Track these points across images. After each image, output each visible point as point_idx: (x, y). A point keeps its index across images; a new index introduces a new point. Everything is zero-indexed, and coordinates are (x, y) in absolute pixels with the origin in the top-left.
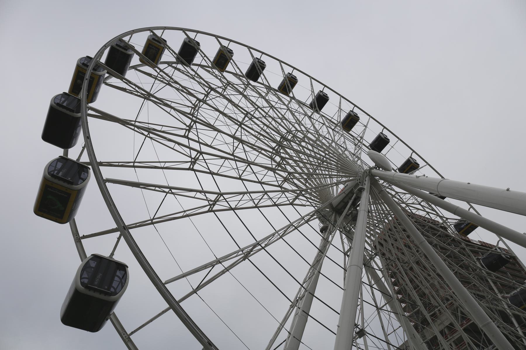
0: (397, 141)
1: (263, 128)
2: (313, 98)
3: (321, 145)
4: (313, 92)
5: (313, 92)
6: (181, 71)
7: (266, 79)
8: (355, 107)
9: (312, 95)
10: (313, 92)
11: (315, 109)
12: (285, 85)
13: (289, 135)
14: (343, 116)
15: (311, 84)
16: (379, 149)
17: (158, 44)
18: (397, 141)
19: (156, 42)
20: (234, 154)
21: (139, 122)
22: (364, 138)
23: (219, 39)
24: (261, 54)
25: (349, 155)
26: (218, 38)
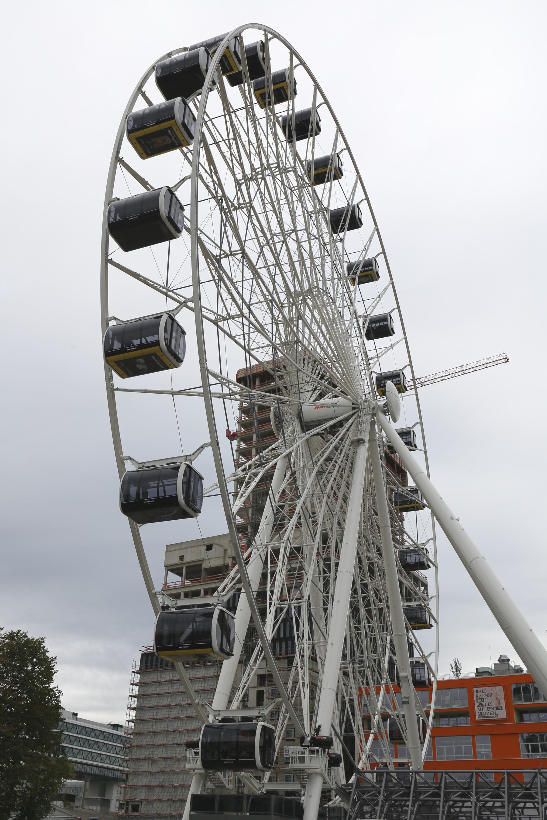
0: (412, 395)
1: (286, 202)
2: (361, 259)
3: (333, 308)
4: (367, 250)
5: (366, 249)
6: (267, 737)
7: (330, 190)
8: (397, 310)
9: (362, 253)
10: (366, 249)
11: (353, 276)
12: (326, 172)
13: (294, 187)
14: (378, 312)
15: (371, 238)
16: (319, 179)
17: (237, 63)
18: (412, 395)
19: (236, 60)
20: (264, 249)
21: (213, 125)
22: (381, 359)
23: (340, 136)
24: (323, 101)
25: (451, 722)
26: (317, 90)
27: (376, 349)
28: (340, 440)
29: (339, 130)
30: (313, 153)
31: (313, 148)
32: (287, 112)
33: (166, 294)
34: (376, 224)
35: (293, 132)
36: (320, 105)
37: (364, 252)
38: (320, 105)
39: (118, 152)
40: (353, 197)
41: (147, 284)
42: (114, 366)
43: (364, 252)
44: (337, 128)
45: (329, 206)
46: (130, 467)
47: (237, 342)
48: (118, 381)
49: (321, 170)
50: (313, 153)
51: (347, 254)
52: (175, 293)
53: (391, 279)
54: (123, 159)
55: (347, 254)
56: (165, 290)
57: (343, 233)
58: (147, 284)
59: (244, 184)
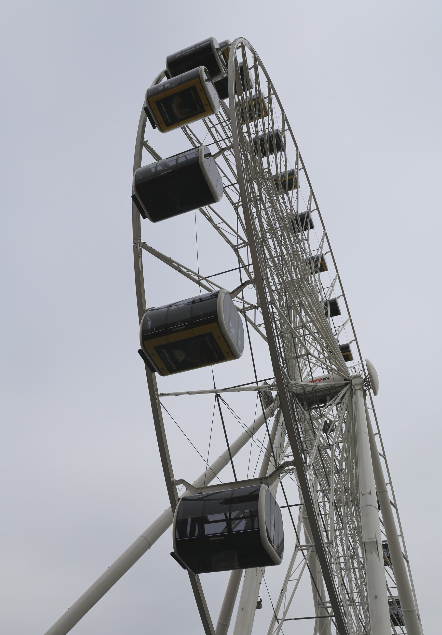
4: (321, 249)
7: (297, 199)
9: (318, 251)
27: (335, 328)
28: (255, 145)
29: (312, 194)
30: (286, 166)
31: (286, 162)
32: (268, 129)
33: (198, 283)
34: (337, 272)
35: (274, 145)
36: (313, 210)
37: (331, 288)
38: (313, 210)
39: (142, 136)
40: (323, 244)
41: (181, 271)
42: (153, 354)
43: (331, 288)
44: (311, 193)
45: (297, 211)
46: (181, 491)
47: (259, 331)
48: (145, 223)
49: (290, 177)
50: (286, 166)
51: (323, 289)
52: (208, 281)
53: (350, 316)
54: (148, 142)
55: (323, 289)
56: (197, 278)
57: (307, 231)
58: (180, 272)
59: (243, 163)
